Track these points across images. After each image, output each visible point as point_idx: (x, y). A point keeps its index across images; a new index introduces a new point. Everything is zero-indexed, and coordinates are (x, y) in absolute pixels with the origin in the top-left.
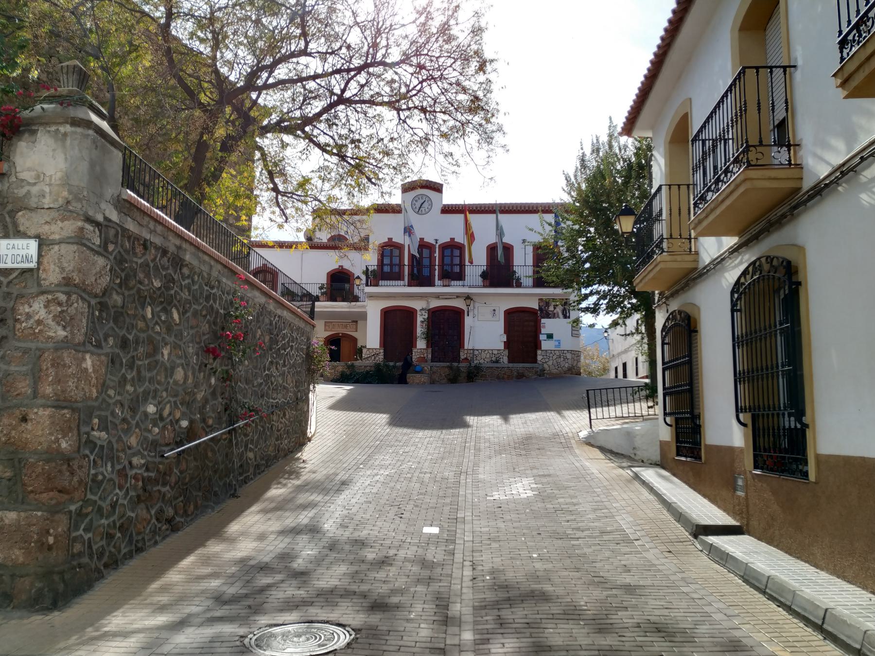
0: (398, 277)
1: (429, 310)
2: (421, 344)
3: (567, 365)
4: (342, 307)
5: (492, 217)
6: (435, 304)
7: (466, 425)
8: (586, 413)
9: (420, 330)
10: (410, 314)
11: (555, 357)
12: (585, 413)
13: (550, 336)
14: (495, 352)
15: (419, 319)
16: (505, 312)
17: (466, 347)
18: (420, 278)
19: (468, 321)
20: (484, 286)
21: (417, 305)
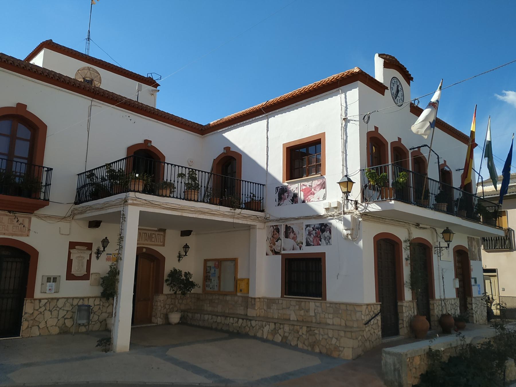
4: (224, 215)
17: (437, 296)
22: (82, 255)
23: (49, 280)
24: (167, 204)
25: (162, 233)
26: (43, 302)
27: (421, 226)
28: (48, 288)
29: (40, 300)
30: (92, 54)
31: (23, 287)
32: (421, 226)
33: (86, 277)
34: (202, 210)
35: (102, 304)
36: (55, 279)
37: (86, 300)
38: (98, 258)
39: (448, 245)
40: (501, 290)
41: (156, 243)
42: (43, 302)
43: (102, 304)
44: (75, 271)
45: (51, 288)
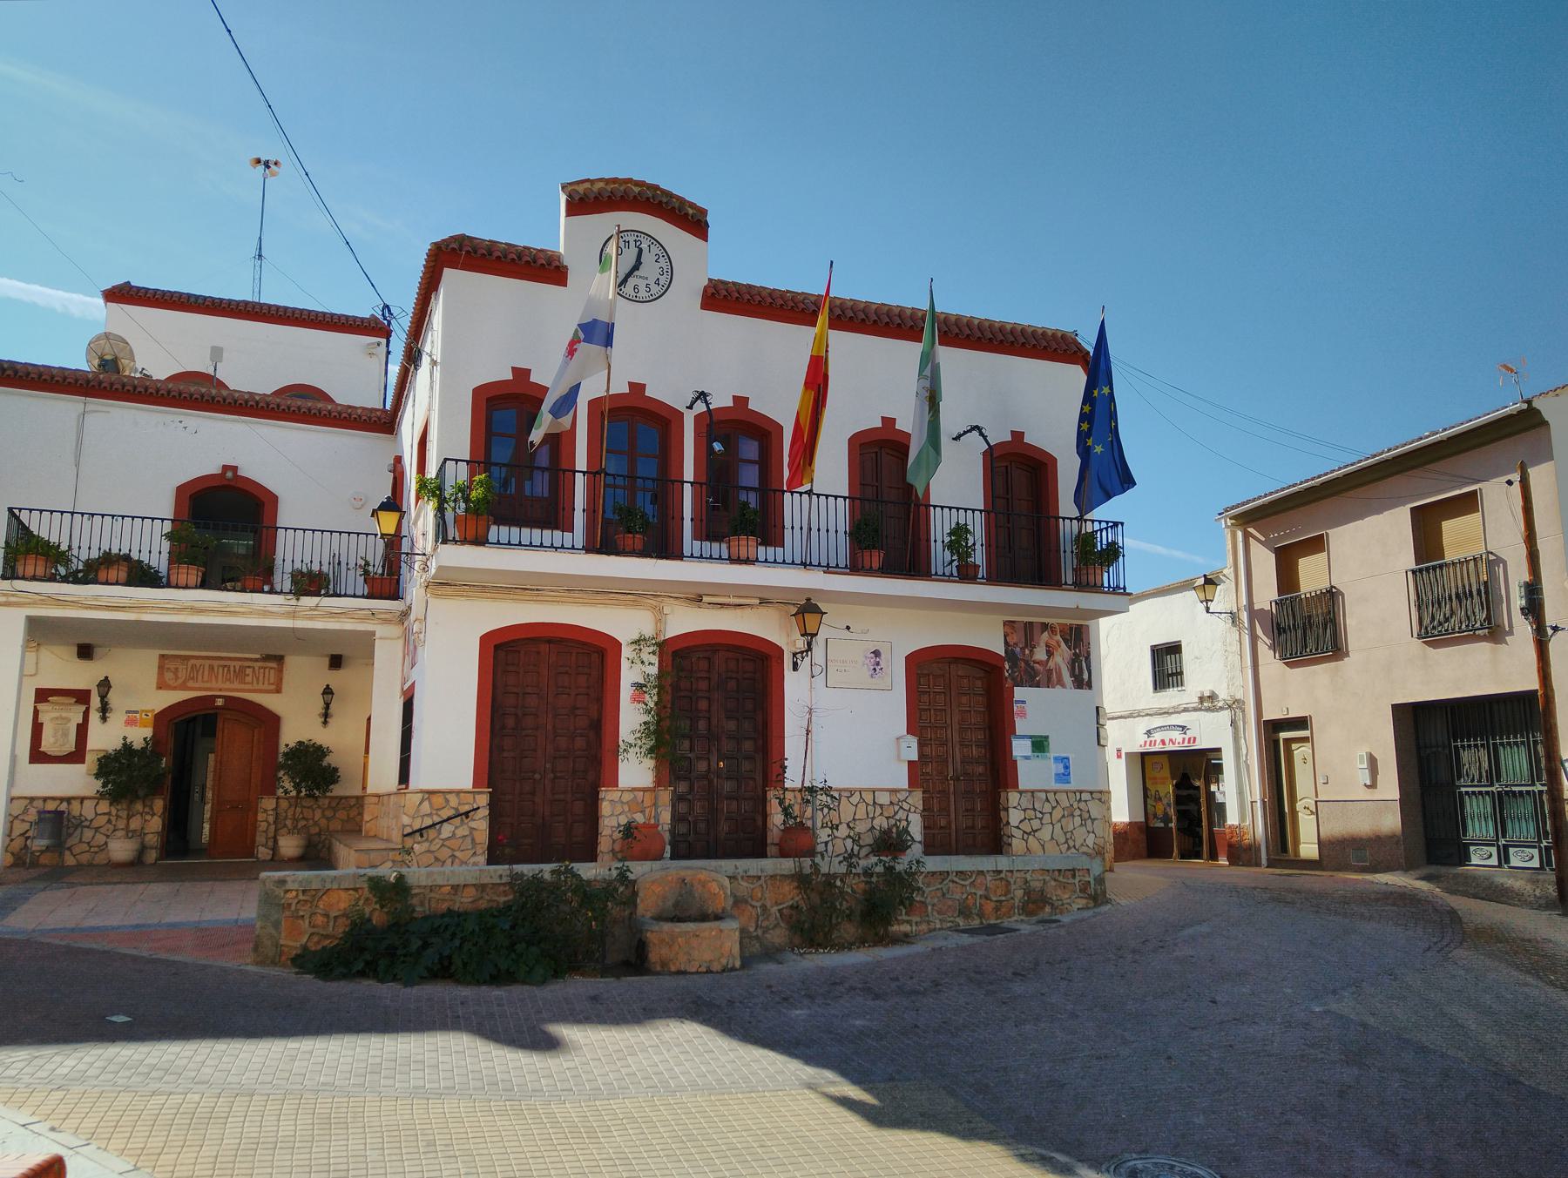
0: (552, 515)
2: (635, 770)
3: (1090, 840)
4: (265, 613)
5: (907, 353)
6: (684, 621)
7: (550, 1044)
9: (631, 718)
10: (597, 654)
11: (1057, 814)
13: (1040, 745)
14: (884, 799)
17: (793, 779)
18: (637, 526)
19: (796, 688)
20: (855, 568)
21: (623, 624)
25: (274, 665)
30: (273, 296)
32: (705, 599)
33: (77, 756)
34: (197, 605)
35: (114, 812)
38: (104, 719)
39: (809, 644)
40: (1320, 780)
41: (256, 686)
43: (114, 812)
44: (48, 744)
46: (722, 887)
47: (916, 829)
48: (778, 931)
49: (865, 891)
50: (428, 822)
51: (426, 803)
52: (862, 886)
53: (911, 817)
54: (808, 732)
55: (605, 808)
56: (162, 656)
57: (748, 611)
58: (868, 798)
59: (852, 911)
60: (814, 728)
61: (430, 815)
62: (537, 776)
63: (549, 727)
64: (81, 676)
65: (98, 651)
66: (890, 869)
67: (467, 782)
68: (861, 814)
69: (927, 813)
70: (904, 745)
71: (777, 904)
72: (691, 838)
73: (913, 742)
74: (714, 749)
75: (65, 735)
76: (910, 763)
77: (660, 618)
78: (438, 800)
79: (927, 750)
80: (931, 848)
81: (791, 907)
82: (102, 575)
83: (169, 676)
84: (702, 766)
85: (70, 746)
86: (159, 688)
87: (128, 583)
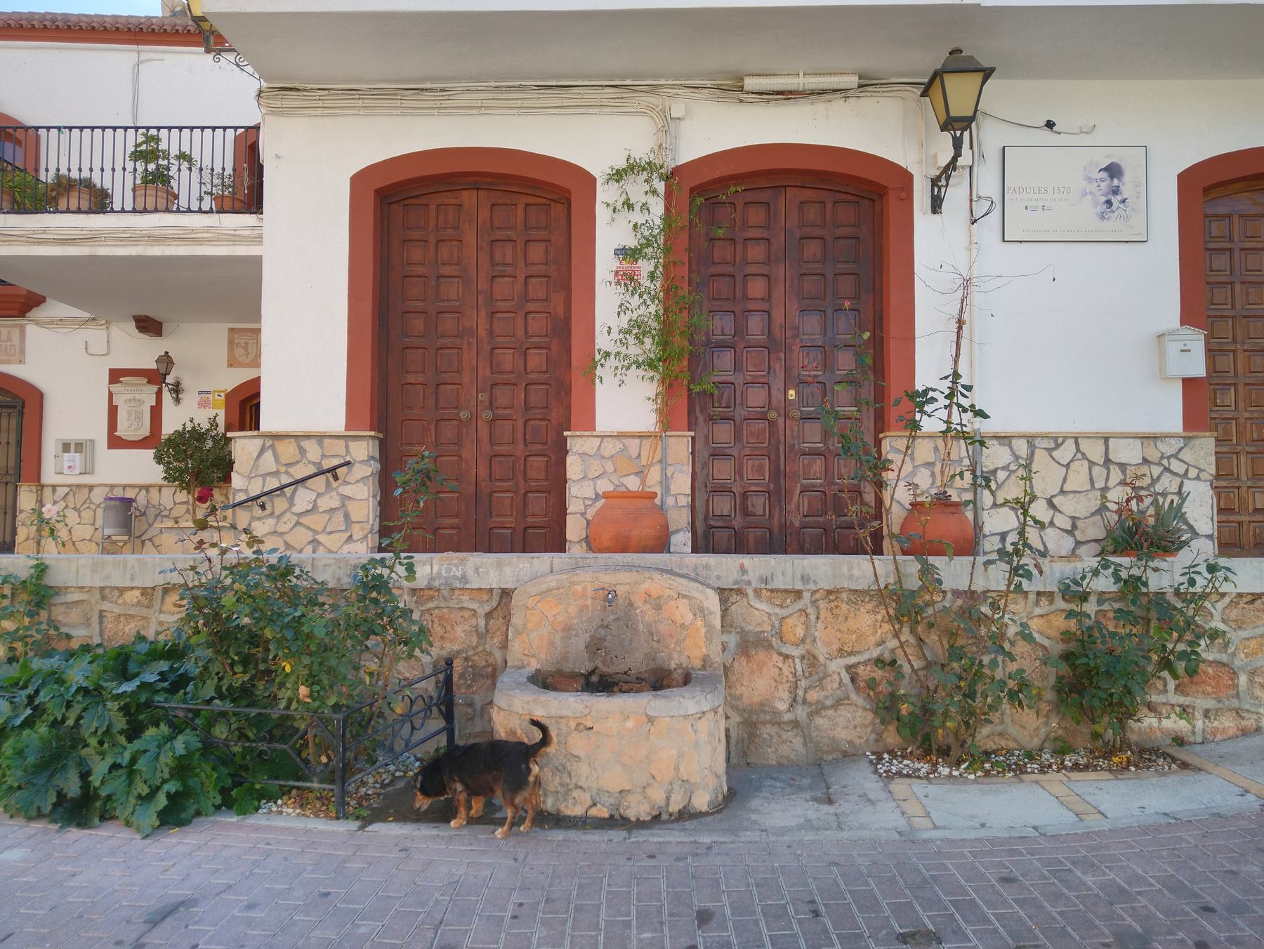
1: (674, 176)
2: (624, 402)
8: (104, 333)
10: (547, 199)
12: (460, 741)
14: (1128, 453)
15: (611, 233)
16: (1187, 180)
19: (937, 245)
22: (137, 396)
23: (66, 447)
24: (46, 230)
26: (61, 492)
27: (750, 83)
28: (66, 465)
29: (54, 487)
31: (25, 464)
34: (156, 233)
36: (79, 446)
37: (154, 492)
38: (177, 400)
42: (61, 492)
45: (70, 464)
46: (700, 611)
47: (1200, 510)
48: (844, 714)
49: (1067, 636)
50: (273, 483)
51: (268, 455)
52: (1060, 622)
53: (1189, 486)
54: (960, 323)
55: (573, 467)
56: (231, 330)
57: (838, 105)
58: (1095, 451)
59: (1024, 685)
60: (977, 322)
61: (276, 474)
62: (464, 415)
63: (482, 332)
64: (144, 352)
65: (166, 327)
66: (1132, 586)
67: (333, 417)
68: (1078, 479)
69: (1223, 478)
70: (1173, 348)
71: (841, 652)
72: (738, 522)
73: (1196, 341)
74: (778, 368)
75: (139, 417)
76: (1188, 383)
77: (667, 124)
78: (287, 450)
79: (1225, 362)
80: (1231, 544)
81: (879, 662)
82: (63, 205)
83: (239, 352)
84: (756, 397)
85: (145, 431)
86: (230, 365)
87: (90, 211)
